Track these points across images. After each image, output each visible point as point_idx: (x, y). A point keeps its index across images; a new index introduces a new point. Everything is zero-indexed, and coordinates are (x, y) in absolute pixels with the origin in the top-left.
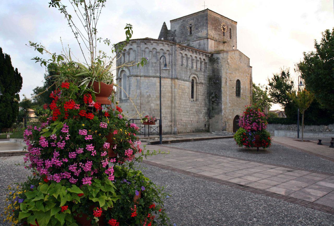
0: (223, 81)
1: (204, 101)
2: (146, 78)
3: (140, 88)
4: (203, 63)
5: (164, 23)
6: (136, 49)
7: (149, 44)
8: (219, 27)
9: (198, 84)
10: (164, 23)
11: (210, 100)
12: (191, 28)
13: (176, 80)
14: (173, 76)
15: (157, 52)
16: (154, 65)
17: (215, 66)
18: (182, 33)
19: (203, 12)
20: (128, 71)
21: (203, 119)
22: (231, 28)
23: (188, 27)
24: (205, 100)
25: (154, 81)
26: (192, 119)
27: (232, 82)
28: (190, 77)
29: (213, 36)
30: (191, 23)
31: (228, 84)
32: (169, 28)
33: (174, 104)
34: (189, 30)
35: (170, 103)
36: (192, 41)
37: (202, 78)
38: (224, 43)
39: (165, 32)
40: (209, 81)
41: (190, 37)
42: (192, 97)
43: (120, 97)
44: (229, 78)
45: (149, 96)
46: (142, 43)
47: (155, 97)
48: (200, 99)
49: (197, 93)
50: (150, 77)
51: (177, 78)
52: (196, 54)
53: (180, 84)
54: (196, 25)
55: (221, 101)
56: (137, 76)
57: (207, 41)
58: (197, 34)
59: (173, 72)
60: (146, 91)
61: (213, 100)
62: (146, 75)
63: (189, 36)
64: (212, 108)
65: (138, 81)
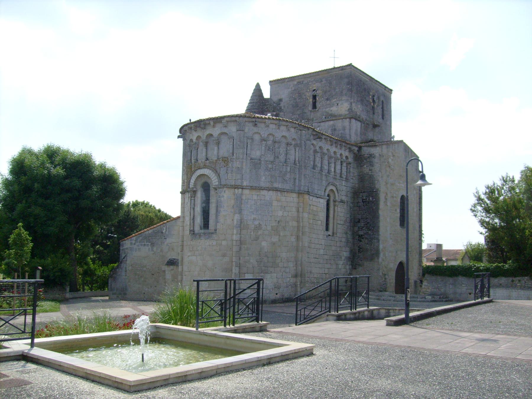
0: (382, 197)
1: (344, 236)
2: (254, 192)
3: (240, 212)
4: (345, 164)
5: (258, 86)
6: (234, 135)
7: (263, 125)
8: (367, 99)
9: (337, 203)
10: (258, 86)
11: (354, 234)
12: (314, 97)
13: (306, 197)
14: (302, 188)
15: (275, 142)
16: (270, 166)
17: (366, 169)
18: (296, 106)
19: (342, 70)
20: (216, 177)
21: (343, 270)
22: (384, 101)
23: (309, 95)
24: (346, 233)
25: (267, 198)
26: (326, 271)
27: (395, 199)
28: (325, 190)
29: (358, 114)
30: (315, 88)
31: (389, 204)
32: (267, 94)
33: (302, 242)
34: (311, 100)
35: (294, 240)
36: (317, 121)
37: (343, 191)
38: (375, 126)
39: (258, 103)
40: (354, 198)
41: (312, 114)
42: (327, 229)
43: (192, 229)
44: (391, 193)
45: (259, 227)
46: (247, 123)
47: (269, 228)
48: (339, 231)
49: (335, 221)
50: (261, 189)
51: (308, 193)
52: (336, 147)
53: (310, 203)
54: (325, 92)
55: (379, 235)
56: (236, 187)
57: (350, 122)
58: (327, 109)
59: (302, 181)
60: (253, 216)
61: (361, 233)
62: (255, 185)
63: (311, 111)
64: (357, 249)
65: (239, 200)
